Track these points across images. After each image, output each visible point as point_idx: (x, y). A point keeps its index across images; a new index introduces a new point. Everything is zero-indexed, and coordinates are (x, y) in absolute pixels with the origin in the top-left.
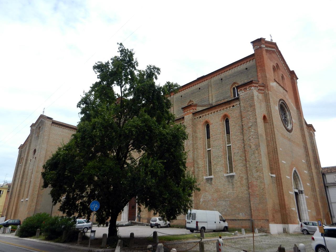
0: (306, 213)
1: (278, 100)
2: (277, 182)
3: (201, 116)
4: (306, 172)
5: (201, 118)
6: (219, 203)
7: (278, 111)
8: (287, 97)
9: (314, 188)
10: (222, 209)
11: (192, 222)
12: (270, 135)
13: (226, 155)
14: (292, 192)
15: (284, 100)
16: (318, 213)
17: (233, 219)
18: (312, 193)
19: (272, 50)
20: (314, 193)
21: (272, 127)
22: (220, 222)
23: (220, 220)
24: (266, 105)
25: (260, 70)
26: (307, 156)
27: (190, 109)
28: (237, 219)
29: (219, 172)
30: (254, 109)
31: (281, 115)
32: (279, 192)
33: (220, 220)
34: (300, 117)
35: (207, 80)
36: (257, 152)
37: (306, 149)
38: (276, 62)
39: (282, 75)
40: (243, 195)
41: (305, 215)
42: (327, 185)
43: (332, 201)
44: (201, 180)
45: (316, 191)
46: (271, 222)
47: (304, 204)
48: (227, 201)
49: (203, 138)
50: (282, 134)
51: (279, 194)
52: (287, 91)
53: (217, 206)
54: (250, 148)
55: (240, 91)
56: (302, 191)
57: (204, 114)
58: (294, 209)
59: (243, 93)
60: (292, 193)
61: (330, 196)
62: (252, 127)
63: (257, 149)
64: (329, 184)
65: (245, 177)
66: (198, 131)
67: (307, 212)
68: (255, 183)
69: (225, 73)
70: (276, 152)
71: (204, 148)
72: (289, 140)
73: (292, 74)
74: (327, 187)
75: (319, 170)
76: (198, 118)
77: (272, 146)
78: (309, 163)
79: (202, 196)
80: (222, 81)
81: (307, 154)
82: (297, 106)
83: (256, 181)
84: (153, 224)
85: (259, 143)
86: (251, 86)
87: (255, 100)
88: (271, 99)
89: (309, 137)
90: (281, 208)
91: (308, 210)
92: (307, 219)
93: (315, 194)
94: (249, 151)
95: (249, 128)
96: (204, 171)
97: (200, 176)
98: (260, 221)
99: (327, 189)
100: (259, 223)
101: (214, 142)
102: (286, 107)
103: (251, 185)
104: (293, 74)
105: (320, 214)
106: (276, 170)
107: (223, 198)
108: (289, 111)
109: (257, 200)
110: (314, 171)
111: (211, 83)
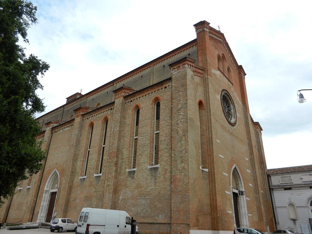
0: (246, 218)
1: (221, 90)
2: (209, 178)
3: (133, 100)
4: (250, 171)
5: (132, 102)
6: (139, 202)
7: (220, 101)
8: (232, 89)
10: (141, 210)
11: (83, 224)
12: (206, 123)
13: (153, 144)
14: (230, 192)
15: (229, 92)
16: (260, 219)
17: (152, 222)
18: (254, 195)
19: (218, 40)
21: (209, 115)
22: (125, 226)
23: (127, 223)
24: (204, 90)
25: (201, 53)
27: (122, 92)
28: (155, 222)
29: (143, 163)
30: (186, 89)
32: (211, 190)
33: (127, 223)
35: (150, 68)
36: (184, 139)
37: (250, 147)
38: (222, 52)
39: (228, 66)
40: (165, 192)
41: (244, 220)
42: (272, 187)
43: (277, 206)
44: (124, 173)
45: (259, 193)
46: (192, 227)
47: (244, 207)
48: (148, 199)
49: (131, 125)
50: (222, 125)
51: (211, 192)
52: (232, 84)
53: (136, 205)
54: (178, 133)
55: (173, 70)
56: (242, 192)
57: (135, 98)
58: (231, 212)
59: (176, 71)
60: (230, 193)
61: (275, 197)
62: (181, 110)
64: (274, 186)
65: (169, 170)
66: (127, 116)
67: (247, 216)
68: (178, 177)
69: (168, 60)
70: (211, 143)
71: (131, 136)
72: (231, 134)
73: (240, 68)
74: (272, 189)
75: (264, 171)
76: (129, 102)
77: (208, 136)
79: (122, 193)
80: (164, 68)
81: (251, 152)
82: (244, 101)
83: (180, 173)
84: (54, 227)
85: (187, 128)
86: (185, 64)
87: (187, 79)
88: (210, 85)
89: (255, 136)
90: (211, 210)
91: (249, 215)
92: (246, 225)
96: (127, 162)
97: (123, 168)
98: (180, 226)
99: (272, 192)
100: (179, 228)
101: (142, 128)
102: (231, 100)
103: (174, 179)
104: (241, 69)
105: (263, 220)
106: (209, 163)
107: (143, 196)
108: (233, 104)
109: (178, 198)
110: (258, 172)
111: (153, 71)
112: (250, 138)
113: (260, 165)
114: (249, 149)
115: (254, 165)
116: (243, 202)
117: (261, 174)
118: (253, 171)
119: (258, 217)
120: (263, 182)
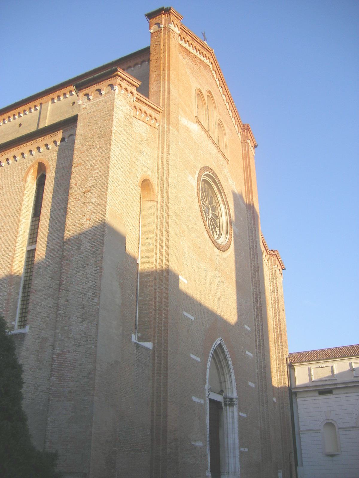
1: (199, 166)
7: (196, 190)
26: (258, 318)
31: (204, 211)
34: (253, 226)
37: (257, 301)
41: (231, 460)
43: (302, 428)
52: (227, 160)
54: (79, 248)
56: (231, 399)
62: (93, 191)
63: (94, 253)
70: (164, 281)
74: (296, 393)
91: (242, 449)
94: (74, 259)
95: (85, 193)
113: (275, 342)
115: (261, 341)
117: (276, 362)
120: (278, 379)
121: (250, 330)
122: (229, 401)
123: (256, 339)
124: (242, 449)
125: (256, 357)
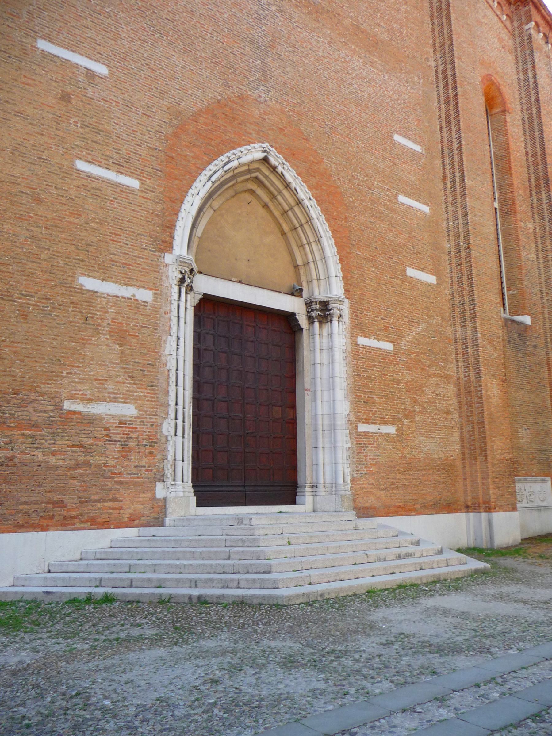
9: (466, 299)
20: (464, 327)
26: (448, 123)
37: (446, 86)
41: (324, 457)
47: (332, 388)
56: (325, 305)
78: (456, 159)
91: (363, 428)
93: (469, 332)
112: (448, 43)
113: (531, 195)
114: (439, 101)
115: (458, 175)
116: (325, 361)
117: (535, 237)
118: (451, 208)
119: (462, 438)
120: (540, 274)
121: (420, 151)
122: (317, 310)
123: (444, 172)
124: (363, 428)
125: (445, 216)
